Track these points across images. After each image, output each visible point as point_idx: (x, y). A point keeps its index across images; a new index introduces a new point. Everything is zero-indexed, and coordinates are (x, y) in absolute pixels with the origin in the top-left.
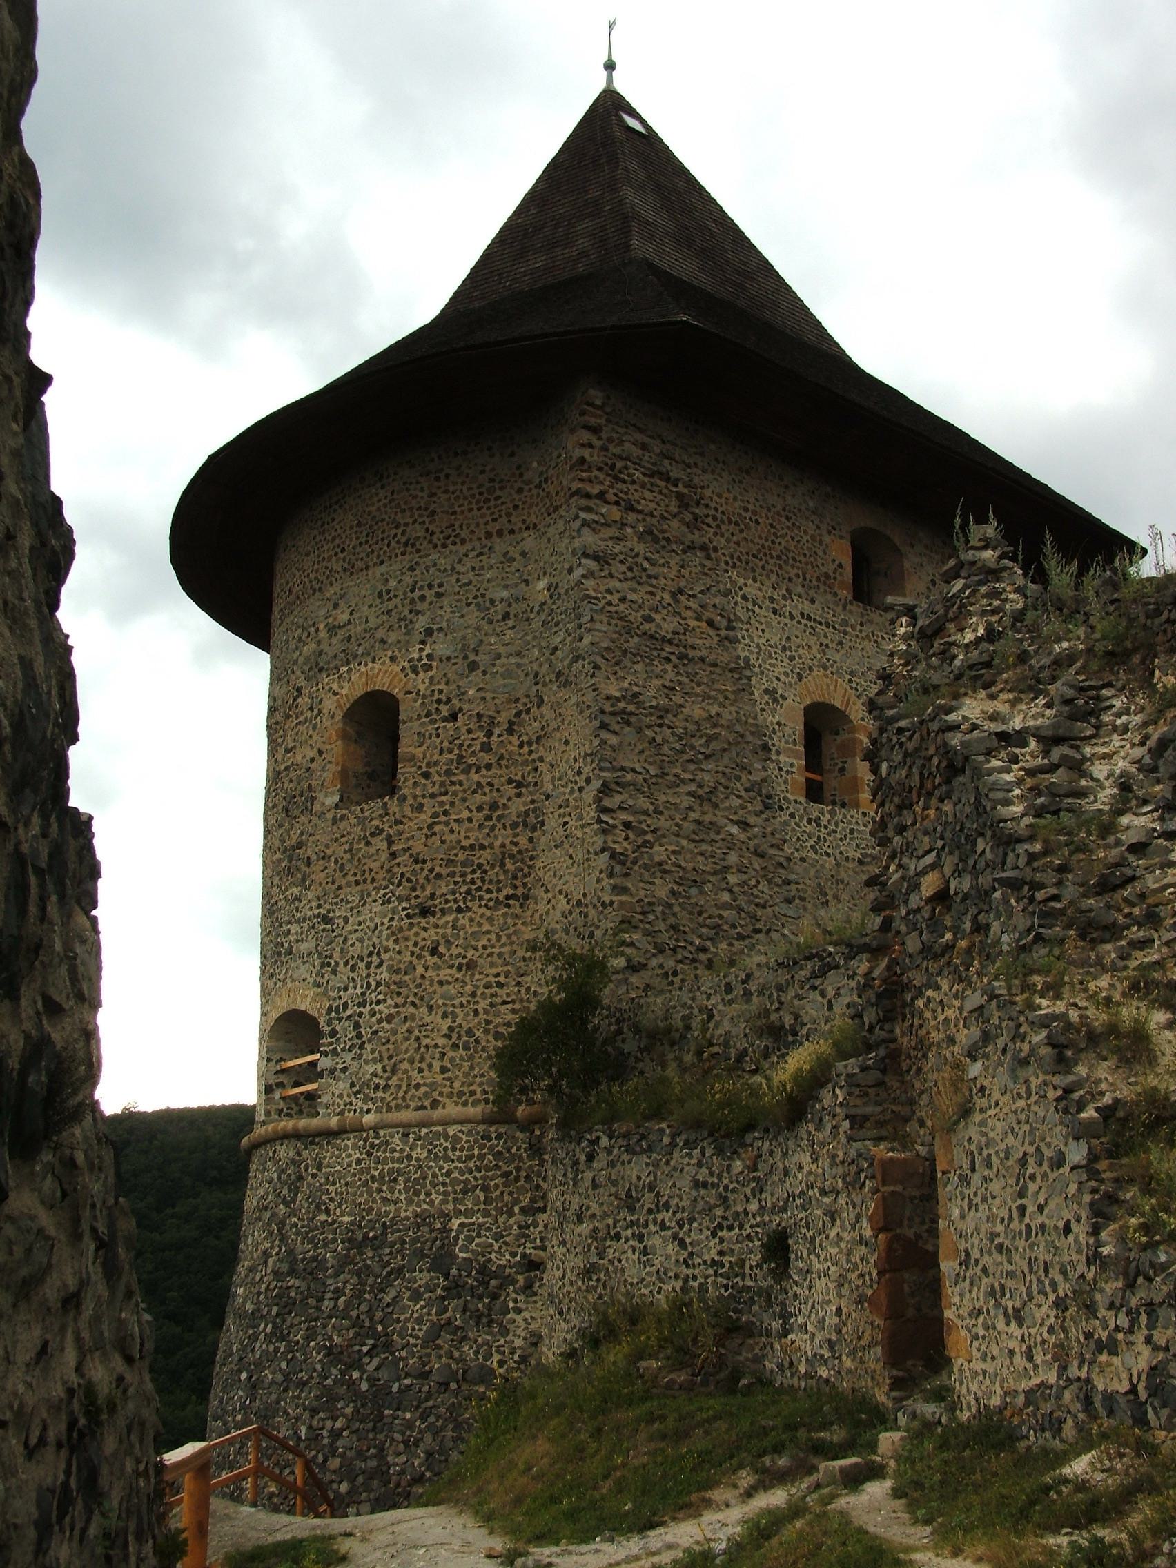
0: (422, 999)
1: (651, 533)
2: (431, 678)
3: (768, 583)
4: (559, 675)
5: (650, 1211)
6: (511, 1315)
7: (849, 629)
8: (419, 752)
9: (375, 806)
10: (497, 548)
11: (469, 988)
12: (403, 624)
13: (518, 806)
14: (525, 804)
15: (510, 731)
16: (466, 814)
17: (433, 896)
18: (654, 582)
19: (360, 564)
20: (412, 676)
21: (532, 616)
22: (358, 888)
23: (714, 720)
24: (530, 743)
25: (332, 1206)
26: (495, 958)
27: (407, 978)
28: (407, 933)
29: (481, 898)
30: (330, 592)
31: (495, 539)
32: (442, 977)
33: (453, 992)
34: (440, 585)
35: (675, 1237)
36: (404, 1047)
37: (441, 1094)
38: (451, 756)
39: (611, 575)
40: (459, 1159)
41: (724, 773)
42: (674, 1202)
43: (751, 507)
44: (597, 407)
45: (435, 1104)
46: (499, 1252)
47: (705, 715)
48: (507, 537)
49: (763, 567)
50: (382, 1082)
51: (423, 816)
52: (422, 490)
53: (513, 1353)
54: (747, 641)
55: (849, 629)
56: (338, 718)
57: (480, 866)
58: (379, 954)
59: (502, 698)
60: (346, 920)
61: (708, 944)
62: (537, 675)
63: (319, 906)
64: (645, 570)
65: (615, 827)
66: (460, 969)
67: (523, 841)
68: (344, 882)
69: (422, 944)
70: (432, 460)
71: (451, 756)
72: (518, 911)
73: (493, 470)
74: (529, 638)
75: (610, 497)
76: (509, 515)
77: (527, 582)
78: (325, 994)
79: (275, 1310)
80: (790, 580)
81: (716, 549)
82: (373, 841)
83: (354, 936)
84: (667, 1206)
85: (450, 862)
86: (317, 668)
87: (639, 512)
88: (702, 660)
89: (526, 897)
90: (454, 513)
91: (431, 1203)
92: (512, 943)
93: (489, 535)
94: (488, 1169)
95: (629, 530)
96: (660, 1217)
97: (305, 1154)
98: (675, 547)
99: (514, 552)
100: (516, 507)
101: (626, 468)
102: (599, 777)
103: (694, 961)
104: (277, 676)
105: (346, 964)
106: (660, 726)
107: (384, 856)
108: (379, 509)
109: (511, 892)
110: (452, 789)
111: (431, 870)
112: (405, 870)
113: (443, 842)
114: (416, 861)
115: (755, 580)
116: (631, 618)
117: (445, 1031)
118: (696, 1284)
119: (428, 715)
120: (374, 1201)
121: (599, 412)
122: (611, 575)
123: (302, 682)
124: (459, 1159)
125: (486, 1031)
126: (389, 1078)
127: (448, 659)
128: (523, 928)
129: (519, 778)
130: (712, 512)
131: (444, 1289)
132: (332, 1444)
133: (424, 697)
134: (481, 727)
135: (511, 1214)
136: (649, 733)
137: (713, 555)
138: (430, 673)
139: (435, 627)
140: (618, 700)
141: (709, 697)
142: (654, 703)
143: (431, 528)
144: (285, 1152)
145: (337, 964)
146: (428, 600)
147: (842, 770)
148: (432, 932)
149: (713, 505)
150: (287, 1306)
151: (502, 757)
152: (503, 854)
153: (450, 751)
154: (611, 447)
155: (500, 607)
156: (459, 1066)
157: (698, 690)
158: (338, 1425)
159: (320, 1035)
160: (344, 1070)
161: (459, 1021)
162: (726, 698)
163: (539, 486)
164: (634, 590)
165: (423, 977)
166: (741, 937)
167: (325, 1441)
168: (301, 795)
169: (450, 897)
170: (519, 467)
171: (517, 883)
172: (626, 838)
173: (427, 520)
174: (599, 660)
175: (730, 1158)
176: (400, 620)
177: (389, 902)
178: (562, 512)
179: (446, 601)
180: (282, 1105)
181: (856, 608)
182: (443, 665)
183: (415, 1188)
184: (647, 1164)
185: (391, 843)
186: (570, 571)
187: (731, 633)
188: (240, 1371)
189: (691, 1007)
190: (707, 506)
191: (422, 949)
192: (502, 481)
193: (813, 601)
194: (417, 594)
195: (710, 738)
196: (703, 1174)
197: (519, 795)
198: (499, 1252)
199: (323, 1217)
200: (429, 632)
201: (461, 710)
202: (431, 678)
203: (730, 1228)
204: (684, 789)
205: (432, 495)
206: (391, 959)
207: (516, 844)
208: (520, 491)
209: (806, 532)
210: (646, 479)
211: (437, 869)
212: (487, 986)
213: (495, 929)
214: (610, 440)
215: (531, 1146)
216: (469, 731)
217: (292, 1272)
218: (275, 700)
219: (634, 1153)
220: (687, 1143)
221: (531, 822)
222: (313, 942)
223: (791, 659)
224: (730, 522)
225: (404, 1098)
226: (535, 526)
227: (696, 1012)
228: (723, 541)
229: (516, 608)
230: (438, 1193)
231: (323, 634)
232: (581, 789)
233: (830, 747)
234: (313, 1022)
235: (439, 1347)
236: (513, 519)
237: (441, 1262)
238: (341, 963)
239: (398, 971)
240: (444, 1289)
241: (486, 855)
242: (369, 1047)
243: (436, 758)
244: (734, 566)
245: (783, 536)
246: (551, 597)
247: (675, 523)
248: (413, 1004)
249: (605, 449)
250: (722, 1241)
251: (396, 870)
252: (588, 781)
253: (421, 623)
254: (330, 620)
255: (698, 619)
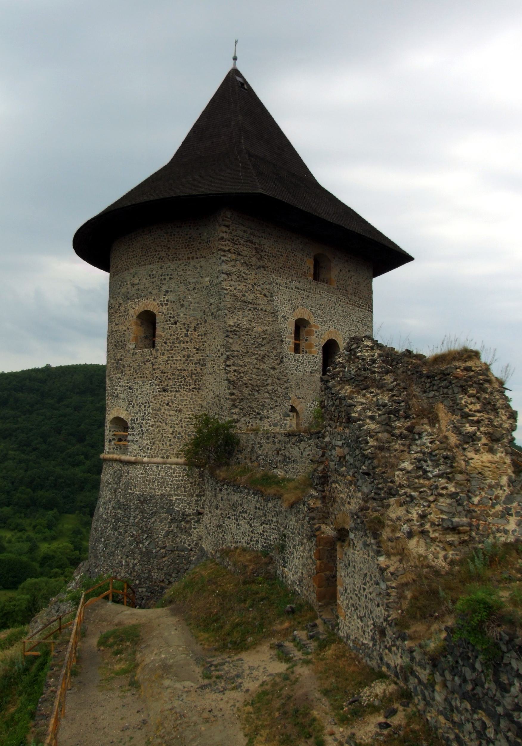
0: (163, 420)
1: (245, 263)
2: (168, 308)
3: (285, 277)
4: (212, 314)
5: (240, 512)
6: (192, 530)
7: (311, 291)
8: (163, 334)
9: (147, 351)
10: (192, 263)
11: (179, 418)
12: (158, 287)
13: (197, 357)
14: (199, 356)
15: (195, 330)
16: (179, 358)
17: (167, 385)
18: (246, 281)
19: (142, 263)
20: (161, 306)
21: (203, 290)
22: (142, 379)
23: (265, 332)
24: (202, 335)
25: (133, 488)
26: (188, 409)
27: (158, 412)
28: (158, 397)
29: (184, 388)
30: (132, 271)
31: (191, 260)
32: (170, 414)
33: (174, 419)
34: (171, 275)
35: (249, 523)
36: (157, 436)
37: (170, 453)
38: (174, 337)
39: (232, 280)
40: (176, 477)
41: (268, 351)
42: (248, 511)
43: (280, 250)
44: (229, 218)
45: (168, 457)
46: (189, 508)
47: (262, 330)
48: (195, 260)
49: (283, 272)
50: (150, 447)
51: (164, 357)
52: (165, 239)
53: (193, 542)
54: (277, 299)
55: (311, 291)
56: (135, 317)
57: (184, 376)
58: (149, 403)
59: (192, 318)
60: (137, 390)
61: (261, 411)
62: (204, 311)
63: (128, 383)
64: (243, 277)
65: (230, 371)
66: (176, 411)
67: (199, 369)
68: (136, 376)
69: (163, 401)
70: (169, 228)
71: (174, 337)
72: (197, 393)
73: (191, 234)
74: (202, 298)
75: (232, 251)
76: (196, 251)
77: (202, 277)
78: (130, 414)
79: (113, 520)
80: (292, 275)
81: (267, 267)
82: (147, 363)
83: (140, 396)
84: (246, 512)
85: (174, 374)
86: (127, 298)
87: (242, 255)
88: (262, 310)
89: (199, 389)
90: (176, 249)
91: (166, 491)
92: (194, 404)
93: (189, 258)
94: (185, 481)
95: (238, 262)
96: (243, 515)
97: (123, 468)
98: (253, 267)
99: (198, 266)
100: (198, 249)
101: (238, 239)
102: (226, 354)
103: (256, 418)
104: (111, 278)
105: (137, 405)
106: (247, 335)
107: (151, 369)
108: (149, 244)
109: (194, 387)
110: (174, 349)
111: (167, 376)
112: (158, 375)
113: (171, 367)
114: (162, 373)
115: (280, 277)
116: (238, 296)
117: (171, 432)
118: (255, 539)
119: (166, 321)
120: (147, 488)
121: (229, 220)
122: (232, 280)
123: (121, 301)
124: (176, 477)
125: (185, 434)
126: (152, 446)
127: (174, 302)
128: (198, 399)
129: (197, 347)
130: (267, 254)
131: (170, 519)
132: (133, 568)
133: (165, 315)
134: (185, 328)
135: (193, 496)
136: (243, 338)
137: (267, 269)
138: (167, 307)
139: (169, 290)
140: (233, 326)
141: (263, 323)
142: (245, 327)
143: (168, 253)
144: (116, 466)
145: (134, 404)
146: (167, 280)
147: (306, 340)
148: (167, 397)
149: (267, 251)
150: (118, 520)
151: (192, 339)
152: (192, 373)
153: (174, 335)
154: (233, 232)
155: (192, 285)
156: (176, 445)
157: (260, 321)
158: (135, 561)
159: (128, 428)
160: (137, 441)
161: (176, 429)
162: (269, 323)
163: (207, 242)
164: (239, 285)
165: (164, 413)
166: (271, 408)
167: (131, 566)
168: (121, 342)
169: (173, 387)
170: (200, 234)
171: (196, 383)
172: (234, 375)
173: (167, 250)
174: (226, 311)
175: (268, 502)
176: (157, 286)
177: (152, 386)
178: (215, 255)
179: (173, 281)
180: (114, 446)
181: (314, 283)
182: (172, 304)
183: (161, 485)
184: (240, 497)
185: (153, 365)
186: (217, 277)
187: (272, 298)
188: (101, 538)
189: (255, 441)
190: (265, 251)
191: (164, 403)
192: (194, 239)
193: (299, 282)
194: (163, 277)
195: (264, 339)
196: (258, 505)
197: (197, 353)
198: (189, 508)
199: (130, 491)
200: (167, 292)
201: (178, 321)
202: (168, 308)
203: (267, 524)
204: (254, 357)
205: (169, 241)
206: (153, 405)
207: (196, 370)
208: (200, 243)
209: (298, 257)
210: (245, 243)
211: (169, 376)
212: (186, 418)
213: (189, 399)
214: (233, 230)
215: (200, 474)
216: (181, 329)
217: (119, 508)
218: (111, 305)
219: (235, 492)
220: (253, 493)
221: (202, 363)
222: (126, 395)
223: (291, 304)
224: (273, 256)
225: (157, 453)
226: (205, 257)
227: (257, 443)
228: (270, 264)
229: (198, 286)
230: (169, 487)
231: (129, 286)
232: (219, 357)
233: (303, 333)
234: (126, 423)
235: (169, 539)
236: (198, 253)
237: (170, 511)
238: (136, 404)
239: (155, 410)
240: (170, 519)
241: (185, 374)
242: (145, 435)
243: (169, 337)
244: (274, 273)
245: (290, 260)
246: (210, 285)
247: (254, 259)
248: (160, 422)
249: (231, 233)
250: (264, 528)
251: (155, 374)
252: (222, 354)
253: (164, 288)
254: (132, 281)
255: (261, 294)
